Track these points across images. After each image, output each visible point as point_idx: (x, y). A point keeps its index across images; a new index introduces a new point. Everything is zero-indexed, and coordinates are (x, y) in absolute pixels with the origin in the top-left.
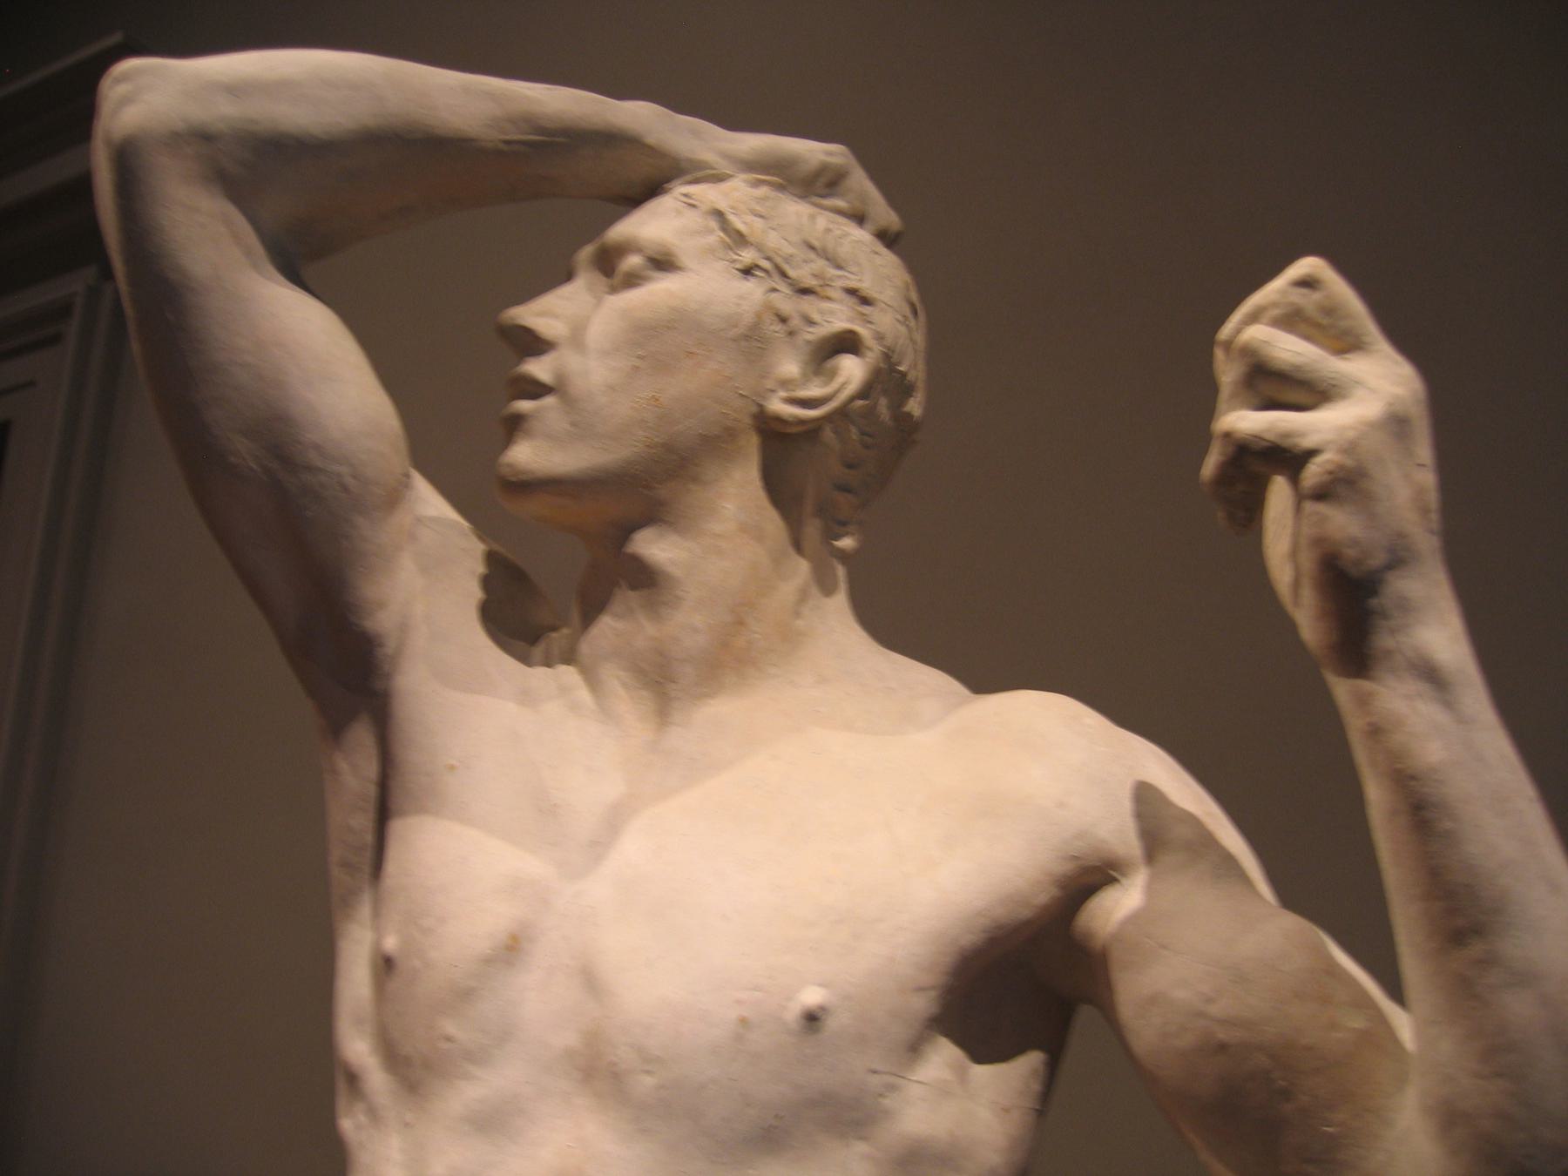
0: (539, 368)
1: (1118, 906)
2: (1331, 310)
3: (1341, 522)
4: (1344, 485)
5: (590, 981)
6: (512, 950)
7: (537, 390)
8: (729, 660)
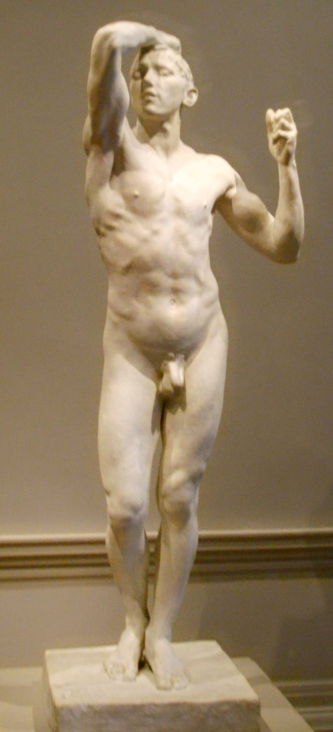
7: (152, 95)
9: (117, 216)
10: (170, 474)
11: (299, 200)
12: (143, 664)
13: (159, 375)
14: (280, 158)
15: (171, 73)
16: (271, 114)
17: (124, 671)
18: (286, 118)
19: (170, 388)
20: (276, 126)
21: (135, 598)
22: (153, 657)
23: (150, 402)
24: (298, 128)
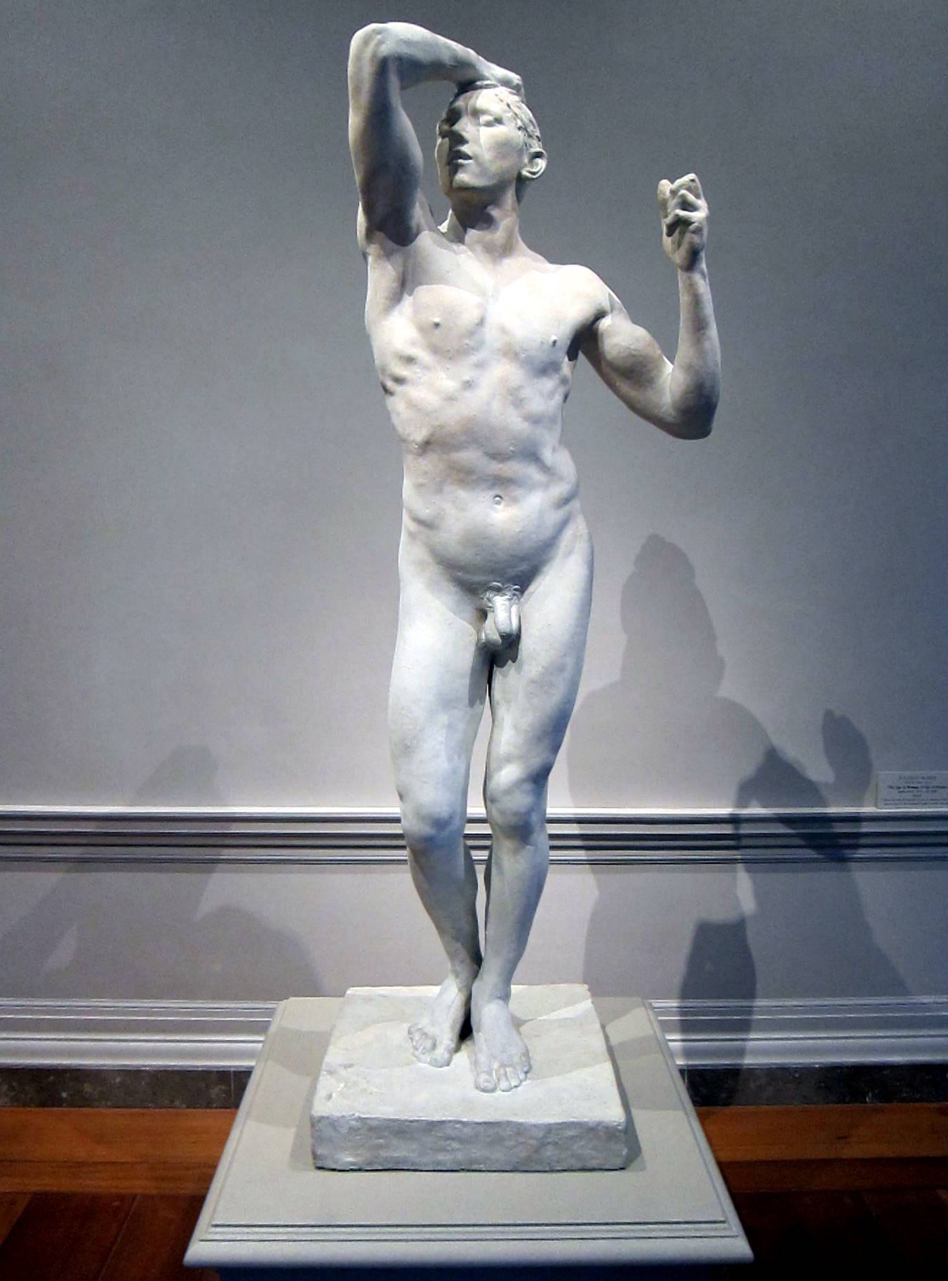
0: (465, 149)
1: (604, 324)
2: (696, 187)
3: (696, 239)
4: (698, 231)
5: (504, 330)
6: (481, 322)
7: (468, 157)
8: (506, 250)
9: (410, 360)
10: (500, 768)
11: (713, 331)
12: (466, 1032)
13: (483, 614)
14: (679, 257)
15: (498, 121)
16: (665, 186)
17: (434, 1046)
18: (689, 189)
19: (496, 637)
20: (672, 203)
21: (457, 939)
22: (478, 1031)
23: (466, 658)
24: (709, 208)
